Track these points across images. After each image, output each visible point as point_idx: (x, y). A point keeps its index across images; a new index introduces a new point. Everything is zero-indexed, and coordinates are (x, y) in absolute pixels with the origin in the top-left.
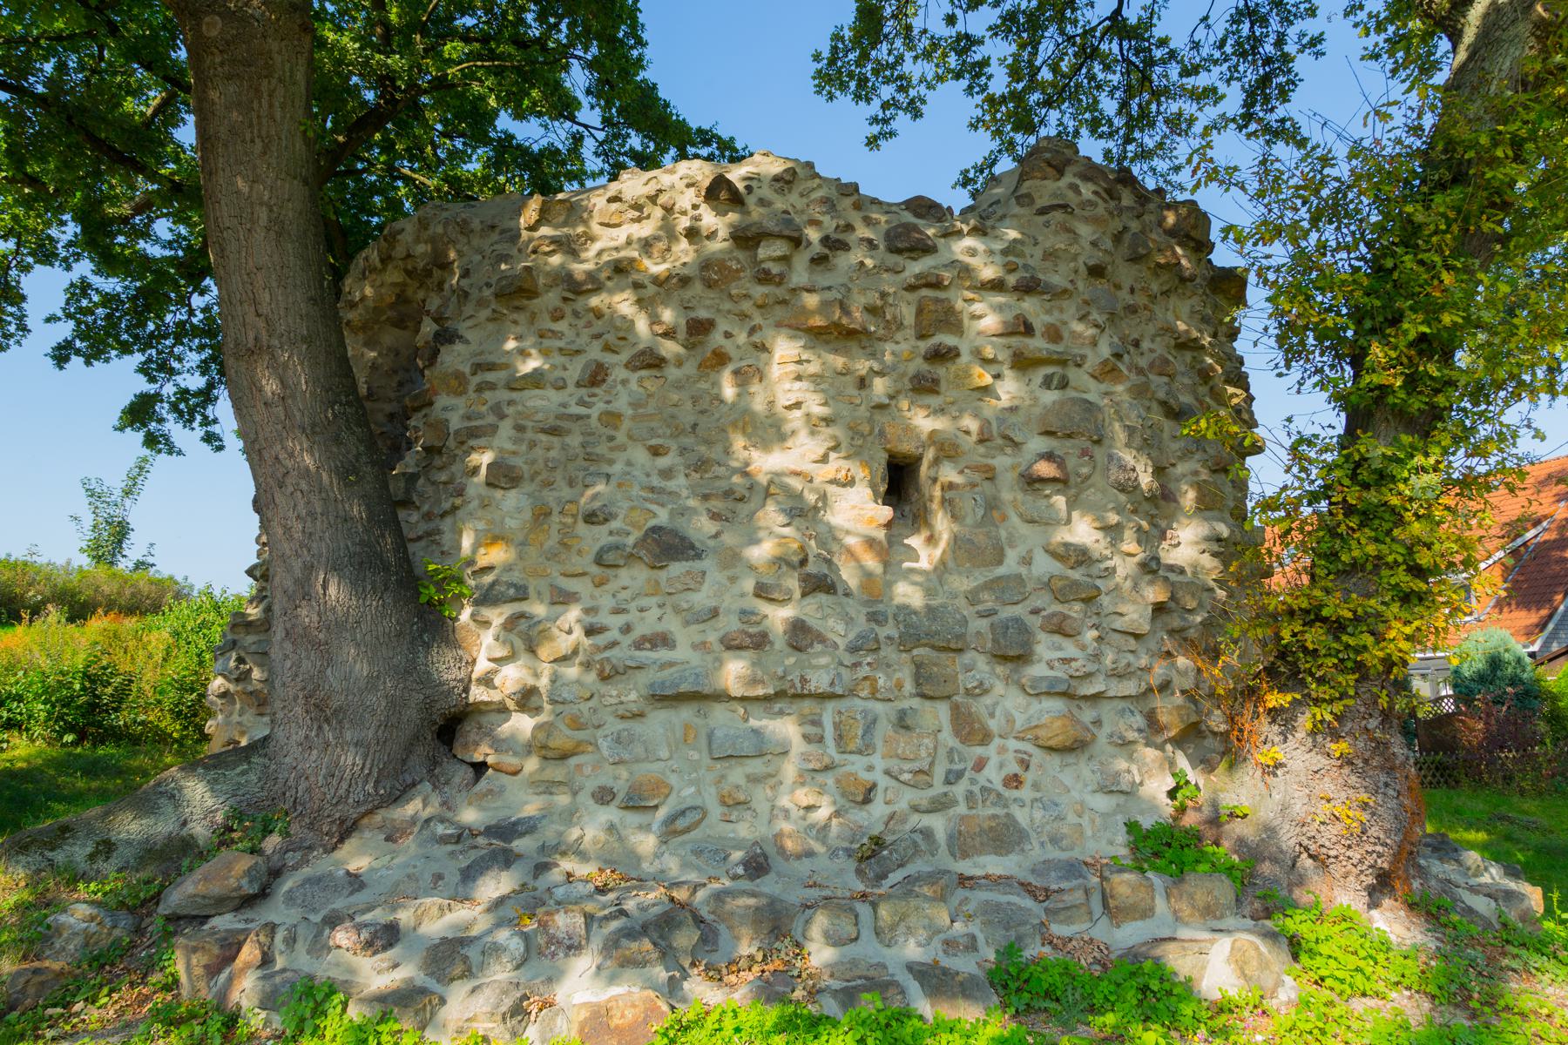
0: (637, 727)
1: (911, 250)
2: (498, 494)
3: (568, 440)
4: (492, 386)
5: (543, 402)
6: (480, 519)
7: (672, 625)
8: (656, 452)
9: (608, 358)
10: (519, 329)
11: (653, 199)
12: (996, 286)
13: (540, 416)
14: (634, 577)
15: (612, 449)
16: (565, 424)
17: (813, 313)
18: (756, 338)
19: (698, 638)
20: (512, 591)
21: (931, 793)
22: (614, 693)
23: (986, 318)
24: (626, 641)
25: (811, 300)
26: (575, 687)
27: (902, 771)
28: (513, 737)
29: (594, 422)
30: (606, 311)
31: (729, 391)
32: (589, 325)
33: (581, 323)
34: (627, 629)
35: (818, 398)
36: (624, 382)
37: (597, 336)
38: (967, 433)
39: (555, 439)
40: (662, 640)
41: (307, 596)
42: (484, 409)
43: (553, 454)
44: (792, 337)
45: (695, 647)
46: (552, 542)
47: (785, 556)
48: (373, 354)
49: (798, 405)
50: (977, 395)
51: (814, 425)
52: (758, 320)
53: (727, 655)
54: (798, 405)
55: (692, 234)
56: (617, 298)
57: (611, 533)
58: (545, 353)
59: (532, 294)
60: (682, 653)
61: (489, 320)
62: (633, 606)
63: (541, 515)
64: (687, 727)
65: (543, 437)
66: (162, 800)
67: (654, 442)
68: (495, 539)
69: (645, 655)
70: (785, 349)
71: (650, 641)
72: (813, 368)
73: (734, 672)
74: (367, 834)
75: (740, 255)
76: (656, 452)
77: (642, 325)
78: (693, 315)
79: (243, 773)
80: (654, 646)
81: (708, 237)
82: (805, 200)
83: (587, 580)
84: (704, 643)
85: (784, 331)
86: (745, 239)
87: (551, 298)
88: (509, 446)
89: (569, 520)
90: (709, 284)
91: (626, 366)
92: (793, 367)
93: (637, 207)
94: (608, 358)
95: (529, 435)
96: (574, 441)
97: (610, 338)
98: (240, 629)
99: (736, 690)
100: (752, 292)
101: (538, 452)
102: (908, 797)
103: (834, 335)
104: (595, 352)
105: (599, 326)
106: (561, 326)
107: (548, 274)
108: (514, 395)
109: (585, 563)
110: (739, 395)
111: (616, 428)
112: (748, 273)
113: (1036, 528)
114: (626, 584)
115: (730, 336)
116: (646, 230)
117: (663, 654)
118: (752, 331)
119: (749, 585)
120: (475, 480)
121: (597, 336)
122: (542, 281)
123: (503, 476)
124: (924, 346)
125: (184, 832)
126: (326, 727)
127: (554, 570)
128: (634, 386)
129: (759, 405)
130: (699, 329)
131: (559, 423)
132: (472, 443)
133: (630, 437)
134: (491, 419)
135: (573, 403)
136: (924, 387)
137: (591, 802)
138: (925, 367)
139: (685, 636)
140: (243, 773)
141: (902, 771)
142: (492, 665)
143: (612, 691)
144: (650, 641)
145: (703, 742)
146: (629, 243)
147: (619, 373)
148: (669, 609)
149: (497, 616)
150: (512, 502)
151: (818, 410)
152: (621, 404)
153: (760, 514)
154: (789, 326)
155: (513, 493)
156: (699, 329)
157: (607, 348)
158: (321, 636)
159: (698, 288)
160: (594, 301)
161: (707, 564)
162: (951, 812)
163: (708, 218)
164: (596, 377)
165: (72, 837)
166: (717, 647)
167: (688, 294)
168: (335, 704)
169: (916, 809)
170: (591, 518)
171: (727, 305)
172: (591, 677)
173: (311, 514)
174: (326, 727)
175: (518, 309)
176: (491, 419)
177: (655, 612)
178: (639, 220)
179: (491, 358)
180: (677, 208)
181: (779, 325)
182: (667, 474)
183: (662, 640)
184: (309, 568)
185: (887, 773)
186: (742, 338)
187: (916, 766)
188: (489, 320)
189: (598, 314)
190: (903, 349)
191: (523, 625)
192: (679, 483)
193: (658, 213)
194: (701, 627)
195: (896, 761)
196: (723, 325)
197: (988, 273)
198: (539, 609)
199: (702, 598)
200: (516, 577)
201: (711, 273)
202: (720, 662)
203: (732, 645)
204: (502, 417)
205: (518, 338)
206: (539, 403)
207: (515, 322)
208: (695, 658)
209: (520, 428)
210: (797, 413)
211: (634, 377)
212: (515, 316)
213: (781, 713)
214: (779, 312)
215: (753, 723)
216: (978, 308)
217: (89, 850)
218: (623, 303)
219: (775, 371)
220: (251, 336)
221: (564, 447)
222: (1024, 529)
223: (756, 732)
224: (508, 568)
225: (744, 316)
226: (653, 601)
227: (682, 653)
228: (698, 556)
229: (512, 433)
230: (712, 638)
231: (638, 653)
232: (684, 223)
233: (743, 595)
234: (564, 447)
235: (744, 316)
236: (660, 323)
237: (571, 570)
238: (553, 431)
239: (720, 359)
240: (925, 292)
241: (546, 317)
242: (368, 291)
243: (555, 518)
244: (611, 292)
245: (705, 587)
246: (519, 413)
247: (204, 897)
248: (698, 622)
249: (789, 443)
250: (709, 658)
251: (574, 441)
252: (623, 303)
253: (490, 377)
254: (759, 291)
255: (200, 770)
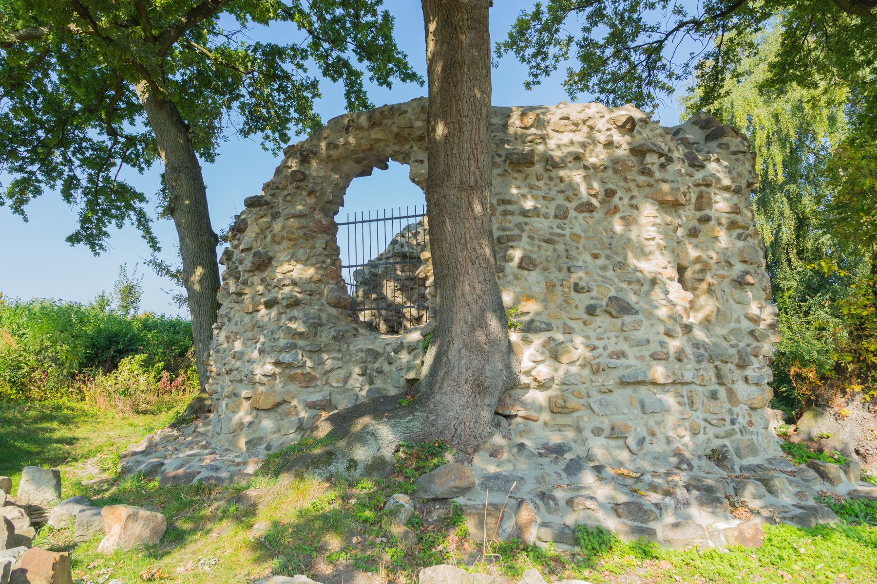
0: (608, 397)
1: (698, 166)
2: (526, 272)
3: (557, 246)
4: (512, 213)
5: (541, 225)
6: (516, 286)
7: (624, 346)
8: (596, 256)
9: (568, 205)
10: (518, 183)
11: (584, 122)
12: (727, 189)
13: (541, 233)
14: (602, 321)
15: (578, 254)
16: (555, 238)
17: (666, 194)
18: (634, 202)
19: (638, 354)
20: (544, 326)
21: (724, 429)
22: (601, 380)
23: (721, 204)
24: (605, 354)
25: (666, 187)
26: (578, 377)
27: (713, 419)
28: (533, 403)
29: (568, 237)
30: (567, 179)
31: (618, 227)
32: (556, 185)
33: (552, 184)
34: (605, 348)
35: (661, 236)
36: (576, 218)
37: (562, 192)
38: (711, 258)
39: (550, 246)
40: (621, 355)
41: (481, 326)
42: (511, 225)
43: (549, 253)
44: (653, 204)
45: (636, 358)
46: (560, 300)
47: (644, 312)
48: (337, 176)
49: (653, 239)
50: (713, 240)
51: (662, 249)
52: (635, 193)
53: (654, 362)
54: (653, 239)
55: (609, 144)
56: (574, 173)
57: (592, 298)
58: (535, 198)
59: (531, 163)
60: (631, 361)
61: (499, 175)
62: (605, 336)
63: (551, 287)
64: (631, 397)
65: (544, 244)
66: (369, 437)
67: (596, 251)
68: (529, 298)
69: (615, 362)
70: (648, 212)
71: (616, 355)
72: (658, 221)
73: (659, 372)
74: (481, 453)
75: (633, 158)
76: (596, 256)
77: (583, 189)
78: (607, 187)
79: (410, 421)
80: (618, 358)
81: (617, 147)
82: (652, 134)
83: (580, 322)
84: (641, 356)
85: (649, 200)
86: (639, 152)
87: (538, 167)
88: (528, 247)
89: (567, 290)
90: (616, 172)
91: (575, 210)
92: (652, 219)
93: (577, 125)
94: (568, 205)
95: (536, 242)
96: (561, 247)
97: (570, 193)
98: (297, 337)
99: (661, 380)
100: (637, 179)
101: (543, 252)
102: (711, 431)
103: (671, 206)
104: (560, 200)
105: (562, 186)
106: (540, 184)
107: (538, 155)
108: (526, 220)
109: (581, 313)
110: (624, 230)
111: (578, 243)
112: (636, 169)
113: (740, 306)
114: (600, 324)
115: (621, 200)
116: (579, 137)
117: (622, 361)
118: (632, 198)
119: (662, 329)
120: (511, 264)
121: (562, 192)
122: (536, 158)
123: (526, 264)
124: (699, 214)
125: (379, 454)
126: (478, 396)
127: (564, 315)
128: (581, 220)
129: (633, 236)
130: (610, 193)
131: (552, 237)
132: (511, 244)
133: (584, 248)
134: (516, 232)
135: (555, 227)
136: (693, 233)
137: (591, 435)
138: (697, 225)
139: (631, 352)
140: (410, 421)
141: (713, 419)
142: (534, 364)
143: (600, 379)
144: (616, 355)
145: (638, 406)
146: (572, 143)
147: (572, 213)
148: (621, 339)
149: (538, 340)
150: (533, 277)
151: (662, 243)
152: (577, 230)
153: (652, 293)
154: (652, 198)
155: (533, 273)
156: (610, 193)
157: (568, 199)
158: (486, 347)
159: (610, 172)
160: (562, 173)
161: (640, 317)
162: (733, 438)
163: (617, 137)
164: (562, 215)
165: (336, 457)
166: (648, 358)
167: (605, 175)
168: (486, 384)
169: (717, 437)
170: (577, 288)
171: (622, 184)
172: (586, 372)
173: (485, 280)
174: (478, 396)
175: (520, 171)
176: (516, 232)
177: (614, 340)
178: (574, 131)
179: (507, 197)
180: (596, 128)
181: (646, 197)
182: (604, 268)
183: (621, 355)
184: (483, 311)
185: (706, 420)
186: (626, 201)
187: (720, 417)
188: (499, 175)
189: (561, 180)
190: (688, 216)
191: (552, 344)
192: (610, 273)
193: (586, 129)
194: (640, 348)
195: (708, 414)
196: (619, 194)
197: (726, 182)
198: (560, 337)
199: (640, 334)
200: (544, 318)
201: (616, 166)
202: (649, 367)
203: (655, 357)
204: (523, 231)
205: (518, 187)
206: (539, 225)
207: (516, 179)
208: (639, 364)
209: (531, 238)
210: (652, 243)
211: (581, 216)
212: (516, 175)
213: (668, 391)
214: (647, 190)
215: (658, 396)
216: (718, 198)
217: (346, 465)
218: (577, 176)
219: (643, 220)
220: (473, 179)
221: (555, 250)
222: (736, 307)
223: (660, 400)
224: (538, 314)
225: (629, 190)
226: (613, 334)
227: (631, 361)
228: (637, 313)
229: (528, 240)
230: (647, 354)
231: (611, 360)
232: (602, 138)
233: (658, 333)
234: (555, 250)
235: (629, 190)
236: (592, 188)
237: (574, 316)
238: (548, 241)
239: (616, 209)
240: (703, 188)
241: (534, 177)
242: (352, 140)
243: (558, 288)
244: (571, 169)
245: (642, 328)
246: (530, 230)
247: (457, 488)
248: (638, 345)
249: (650, 257)
250: (644, 364)
251: (561, 247)
252: (577, 176)
253: (509, 208)
254: (642, 179)
255: (385, 419)
